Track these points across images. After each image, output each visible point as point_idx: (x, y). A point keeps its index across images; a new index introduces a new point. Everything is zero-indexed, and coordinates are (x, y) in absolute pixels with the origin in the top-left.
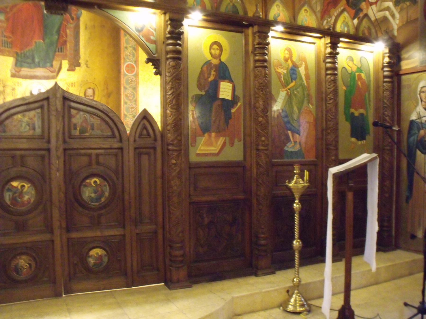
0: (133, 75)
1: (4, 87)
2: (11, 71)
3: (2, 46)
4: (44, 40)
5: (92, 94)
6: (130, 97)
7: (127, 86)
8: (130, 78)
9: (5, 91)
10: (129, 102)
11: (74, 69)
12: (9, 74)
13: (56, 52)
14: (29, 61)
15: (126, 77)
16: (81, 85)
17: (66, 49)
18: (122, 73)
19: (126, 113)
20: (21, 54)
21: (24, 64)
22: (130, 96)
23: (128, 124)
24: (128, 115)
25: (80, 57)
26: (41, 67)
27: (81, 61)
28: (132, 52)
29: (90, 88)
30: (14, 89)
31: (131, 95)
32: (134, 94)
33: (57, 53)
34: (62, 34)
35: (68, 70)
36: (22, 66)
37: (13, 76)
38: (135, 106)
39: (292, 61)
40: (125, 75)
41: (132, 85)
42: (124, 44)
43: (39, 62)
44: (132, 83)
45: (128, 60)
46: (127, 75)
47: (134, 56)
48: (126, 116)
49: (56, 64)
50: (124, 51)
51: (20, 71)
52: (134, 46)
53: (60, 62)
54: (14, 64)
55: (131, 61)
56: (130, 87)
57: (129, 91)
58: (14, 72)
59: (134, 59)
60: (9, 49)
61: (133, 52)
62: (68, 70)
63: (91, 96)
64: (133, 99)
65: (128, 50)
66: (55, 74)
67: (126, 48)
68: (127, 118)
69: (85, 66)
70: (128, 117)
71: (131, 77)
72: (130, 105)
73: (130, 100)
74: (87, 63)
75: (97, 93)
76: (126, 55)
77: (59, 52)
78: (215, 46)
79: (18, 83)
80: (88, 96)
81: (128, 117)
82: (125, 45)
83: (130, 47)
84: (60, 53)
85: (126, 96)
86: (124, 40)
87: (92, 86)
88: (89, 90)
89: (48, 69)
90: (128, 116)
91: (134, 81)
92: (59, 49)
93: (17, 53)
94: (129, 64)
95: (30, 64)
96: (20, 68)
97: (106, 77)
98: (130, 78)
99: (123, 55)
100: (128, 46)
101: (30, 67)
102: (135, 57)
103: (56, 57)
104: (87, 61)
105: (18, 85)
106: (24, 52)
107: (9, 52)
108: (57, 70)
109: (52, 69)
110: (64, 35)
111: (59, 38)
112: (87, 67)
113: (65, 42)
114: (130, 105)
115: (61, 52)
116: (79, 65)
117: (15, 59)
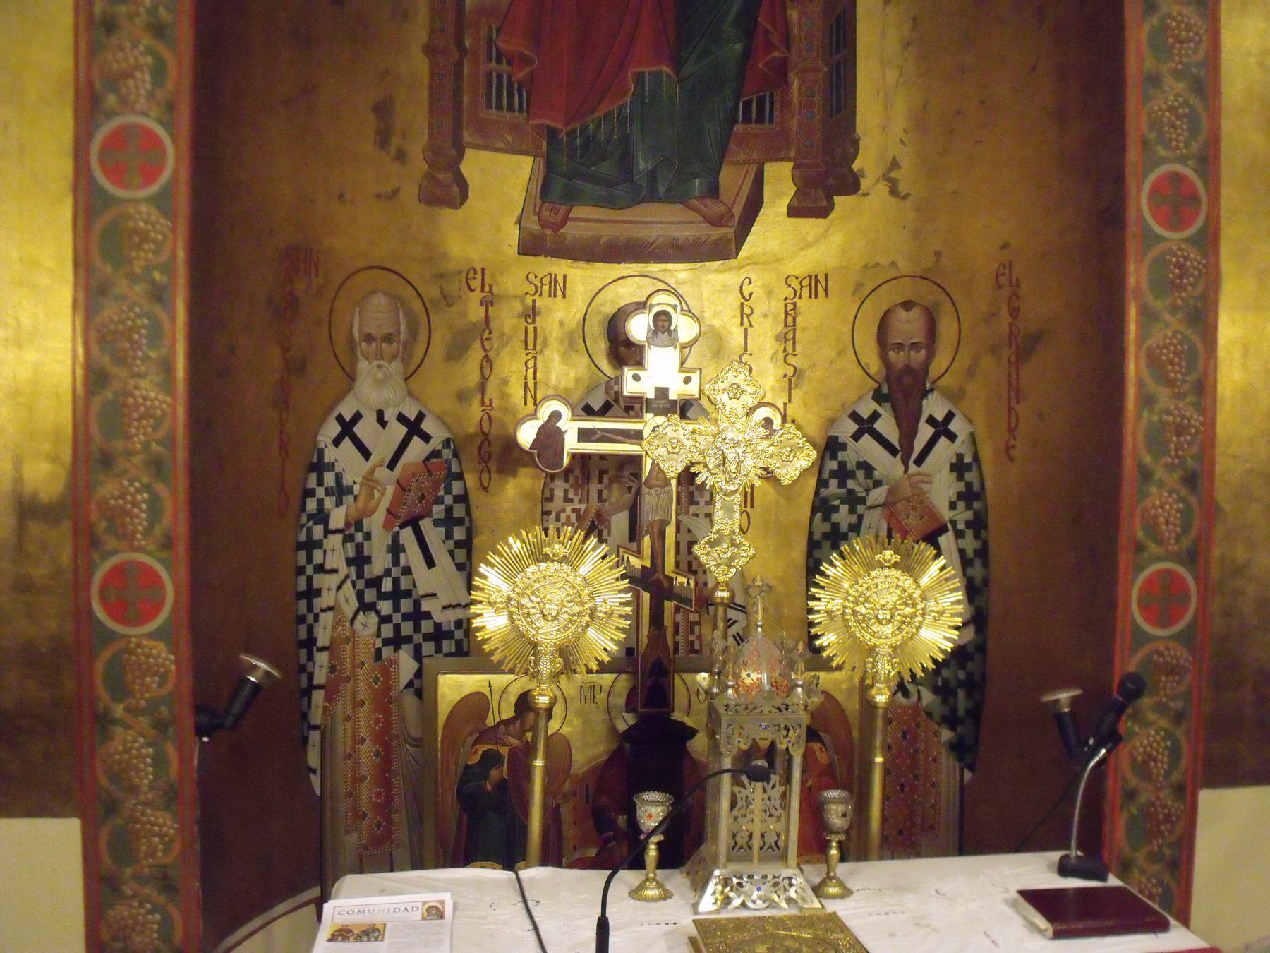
0: (1191, 241)
1: (487, 303)
2: (519, 221)
3: (489, 106)
4: (677, 65)
5: (919, 338)
6: (1170, 367)
7: (1158, 305)
8: (1175, 255)
9: (493, 325)
10: (1163, 396)
11: (824, 203)
12: (512, 235)
13: (734, 121)
14: (606, 169)
15: (1156, 251)
16: (859, 286)
17: (786, 104)
18: (1132, 228)
19: (1147, 459)
20: (571, 134)
21: (588, 187)
22: (1172, 363)
23: (1157, 524)
24: (1159, 473)
25: (856, 144)
26: (660, 200)
27: (866, 162)
28: (1186, 103)
29: (907, 305)
30: (531, 313)
31: (1176, 354)
32: (1193, 348)
33: (739, 128)
34: (767, 32)
35: (793, 212)
36: (572, 198)
37: (531, 247)
38: (1196, 418)
40: (1150, 239)
41: (1183, 295)
42: (1141, 59)
43: (652, 175)
44: (1182, 288)
45: (1162, 152)
46: (1159, 239)
47: (1194, 130)
48: (1146, 475)
49: (732, 180)
50: (1145, 99)
51: (565, 220)
52: (1194, 70)
53: (753, 170)
54: (537, 187)
55: (1181, 160)
56: (1174, 309)
57: (1170, 328)
58: (533, 225)
59: (1195, 146)
60: (519, 118)
61: (1190, 106)
62: (793, 212)
63: (914, 346)
64: (1188, 379)
65: (1163, 92)
66: (729, 232)
67: (1154, 80)
68: (1154, 490)
69: (883, 188)
70: (1160, 484)
71: (1180, 249)
72: (1169, 413)
73: (1171, 383)
74: (893, 174)
75: (947, 329)
76: (1155, 125)
77: (747, 119)
79: (553, 280)
80: (900, 346)
81: (1160, 484)
82: (1149, 64)
83: (1178, 75)
84: (754, 128)
85: (1153, 360)
86: (1144, 37)
87: (926, 292)
88: (902, 314)
89: (695, 210)
90: (1157, 477)
91: (1192, 276)
92: (747, 105)
93: (552, 135)
94: (105, 169)
95: (609, 184)
96: (563, 209)
97: (1005, 246)
98: (1175, 255)
99: (1137, 120)
100: (1165, 68)
101: (610, 202)
102: (1202, 136)
103: (732, 146)
104: (895, 164)
105: (553, 294)
106: (584, 128)
107: (514, 128)
108: (738, 211)
109: (716, 209)
110: (775, 39)
111: (747, 53)
112: (894, 192)
113: (782, 69)
114: (1169, 413)
115: (760, 120)
116: (851, 185)
117: (541, 162)
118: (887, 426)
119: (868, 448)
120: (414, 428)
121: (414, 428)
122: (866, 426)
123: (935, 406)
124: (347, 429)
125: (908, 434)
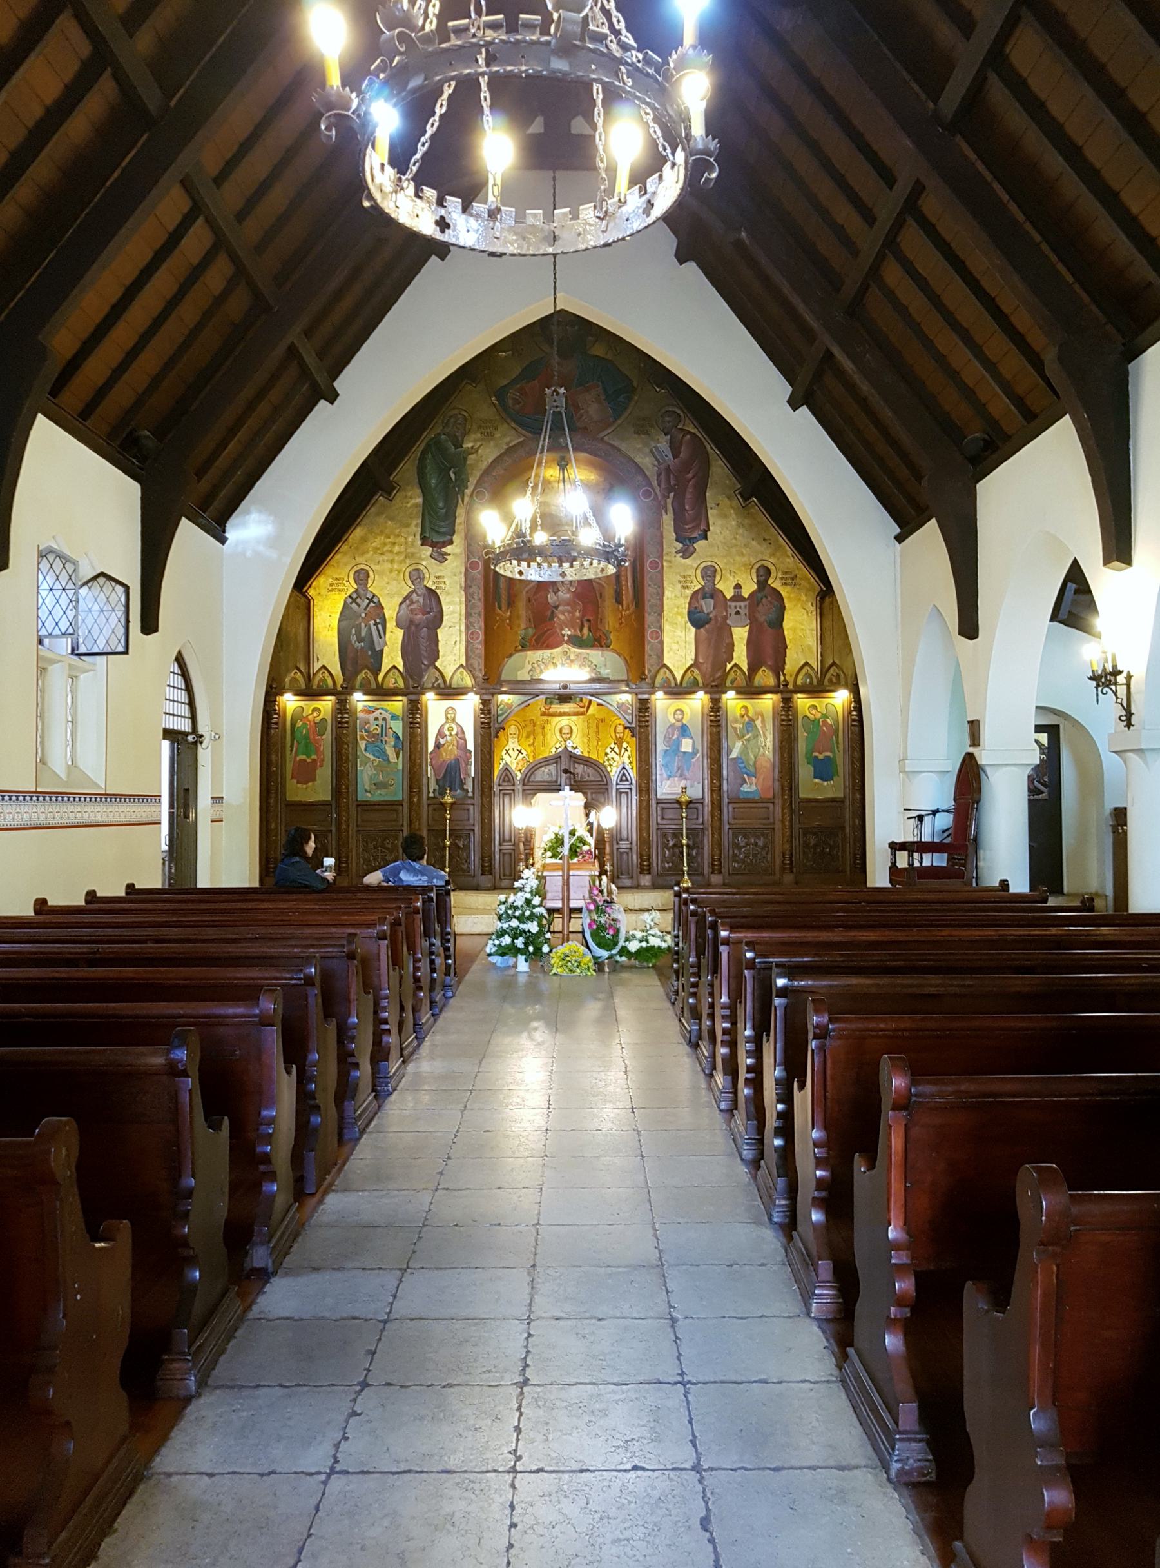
39: (748, 716)
78: (678, 712)
118: (616, 750)
119: (612, 755)
120: (520, 752)
121: (520, 752)
122: (612, 750)
123: (625, 745)
124: (507, 752)
125: (620, 751)
